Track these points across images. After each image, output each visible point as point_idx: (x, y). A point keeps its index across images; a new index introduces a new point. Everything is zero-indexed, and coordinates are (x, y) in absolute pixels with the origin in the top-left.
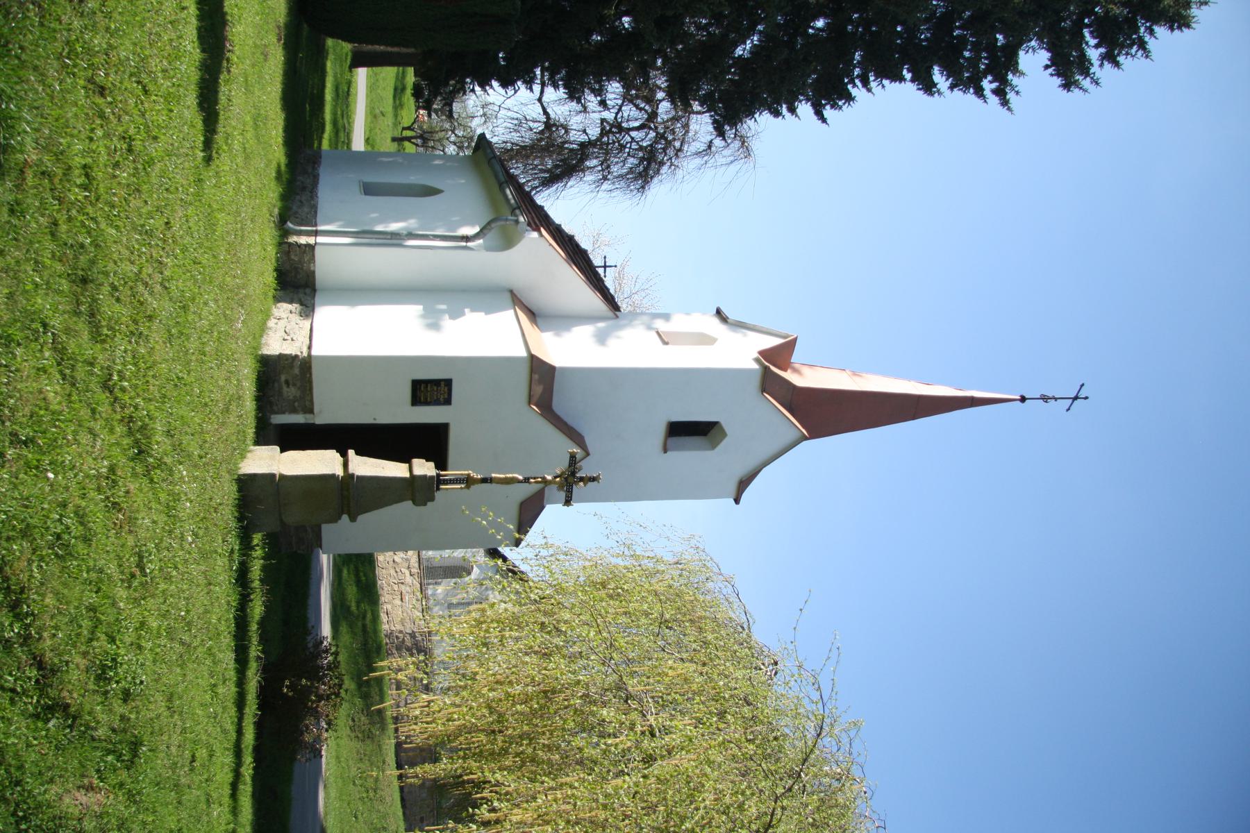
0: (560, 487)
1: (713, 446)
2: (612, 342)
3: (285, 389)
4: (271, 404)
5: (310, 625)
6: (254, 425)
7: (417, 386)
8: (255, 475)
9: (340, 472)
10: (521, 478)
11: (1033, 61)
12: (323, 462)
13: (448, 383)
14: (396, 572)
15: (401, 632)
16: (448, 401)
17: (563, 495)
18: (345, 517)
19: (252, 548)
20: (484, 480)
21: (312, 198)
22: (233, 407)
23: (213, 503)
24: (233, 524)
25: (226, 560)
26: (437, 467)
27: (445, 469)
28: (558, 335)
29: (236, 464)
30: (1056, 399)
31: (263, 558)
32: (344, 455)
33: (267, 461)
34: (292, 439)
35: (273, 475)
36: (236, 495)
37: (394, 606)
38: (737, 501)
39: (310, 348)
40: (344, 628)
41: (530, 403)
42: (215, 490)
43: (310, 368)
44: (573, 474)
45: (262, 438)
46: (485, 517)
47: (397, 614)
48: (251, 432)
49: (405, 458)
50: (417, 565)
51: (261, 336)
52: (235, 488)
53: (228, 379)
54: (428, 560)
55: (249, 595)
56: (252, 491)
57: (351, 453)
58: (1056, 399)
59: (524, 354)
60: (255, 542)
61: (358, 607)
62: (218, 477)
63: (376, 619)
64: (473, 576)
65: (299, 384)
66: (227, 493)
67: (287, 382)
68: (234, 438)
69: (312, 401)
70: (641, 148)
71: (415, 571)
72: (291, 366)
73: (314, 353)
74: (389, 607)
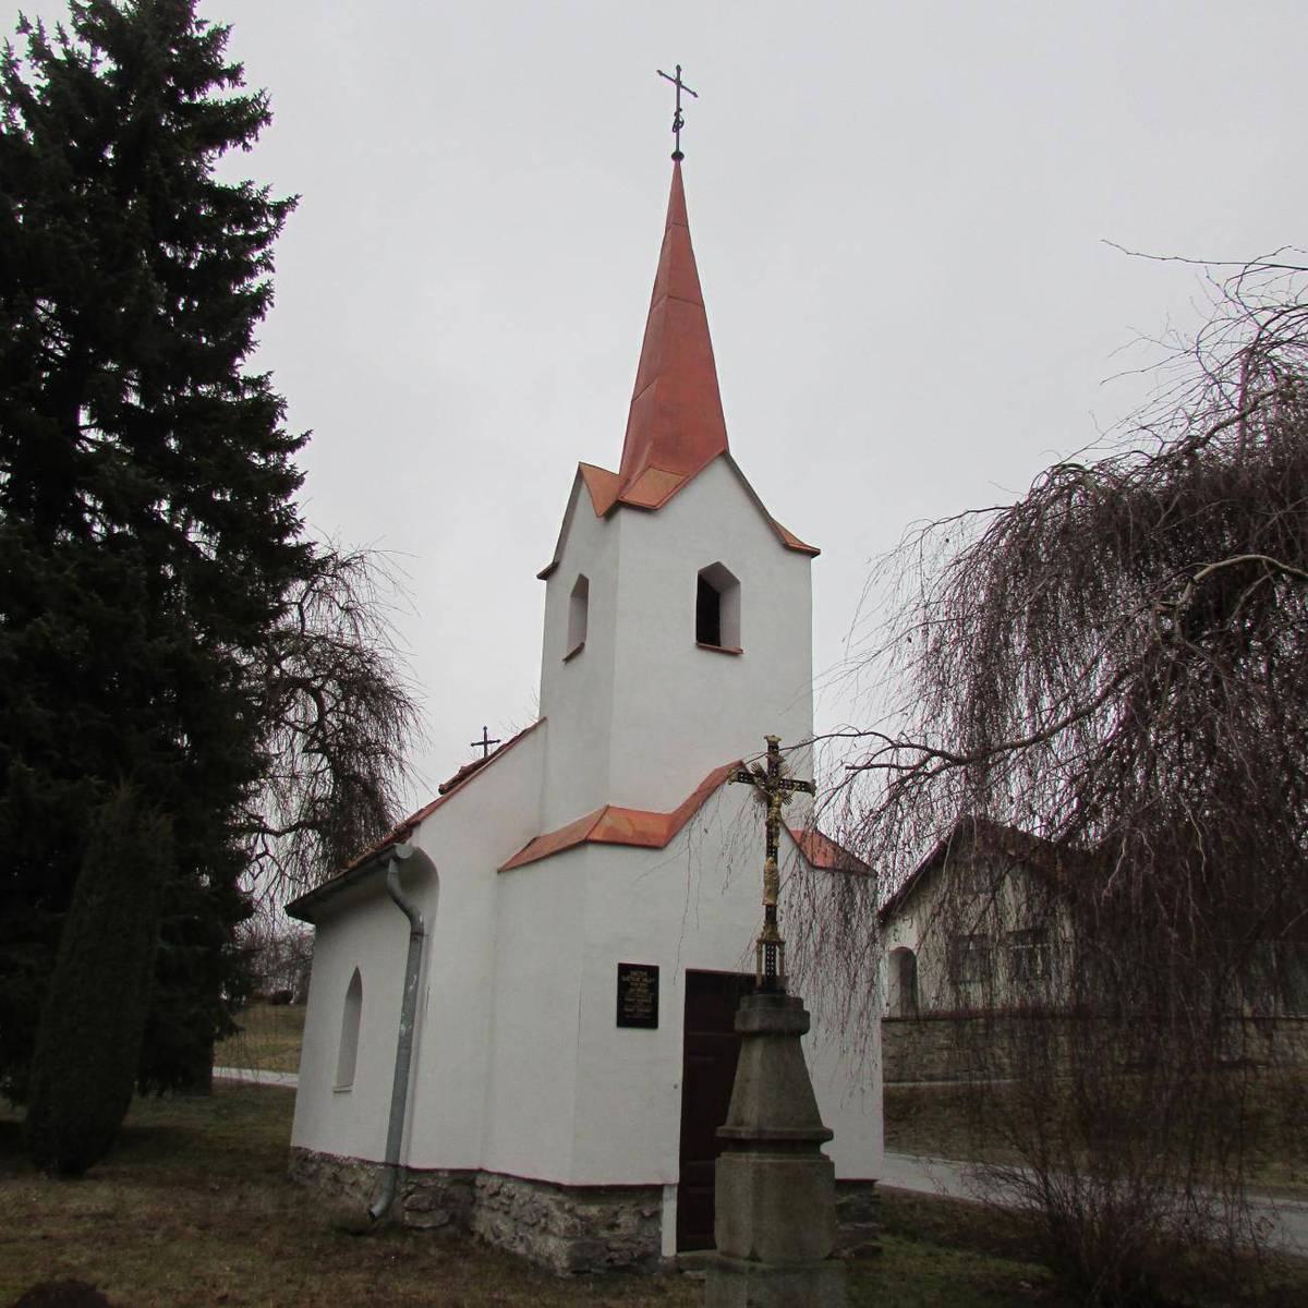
1: (732, 582)
11: (226, 168)
13: (624, 969)
16: (653, 972)
18: (825, 1148)
21: (350, 1167)
30: (679, 110)
38: (814, 553)
58: (679, 110)
70: (345, 698)
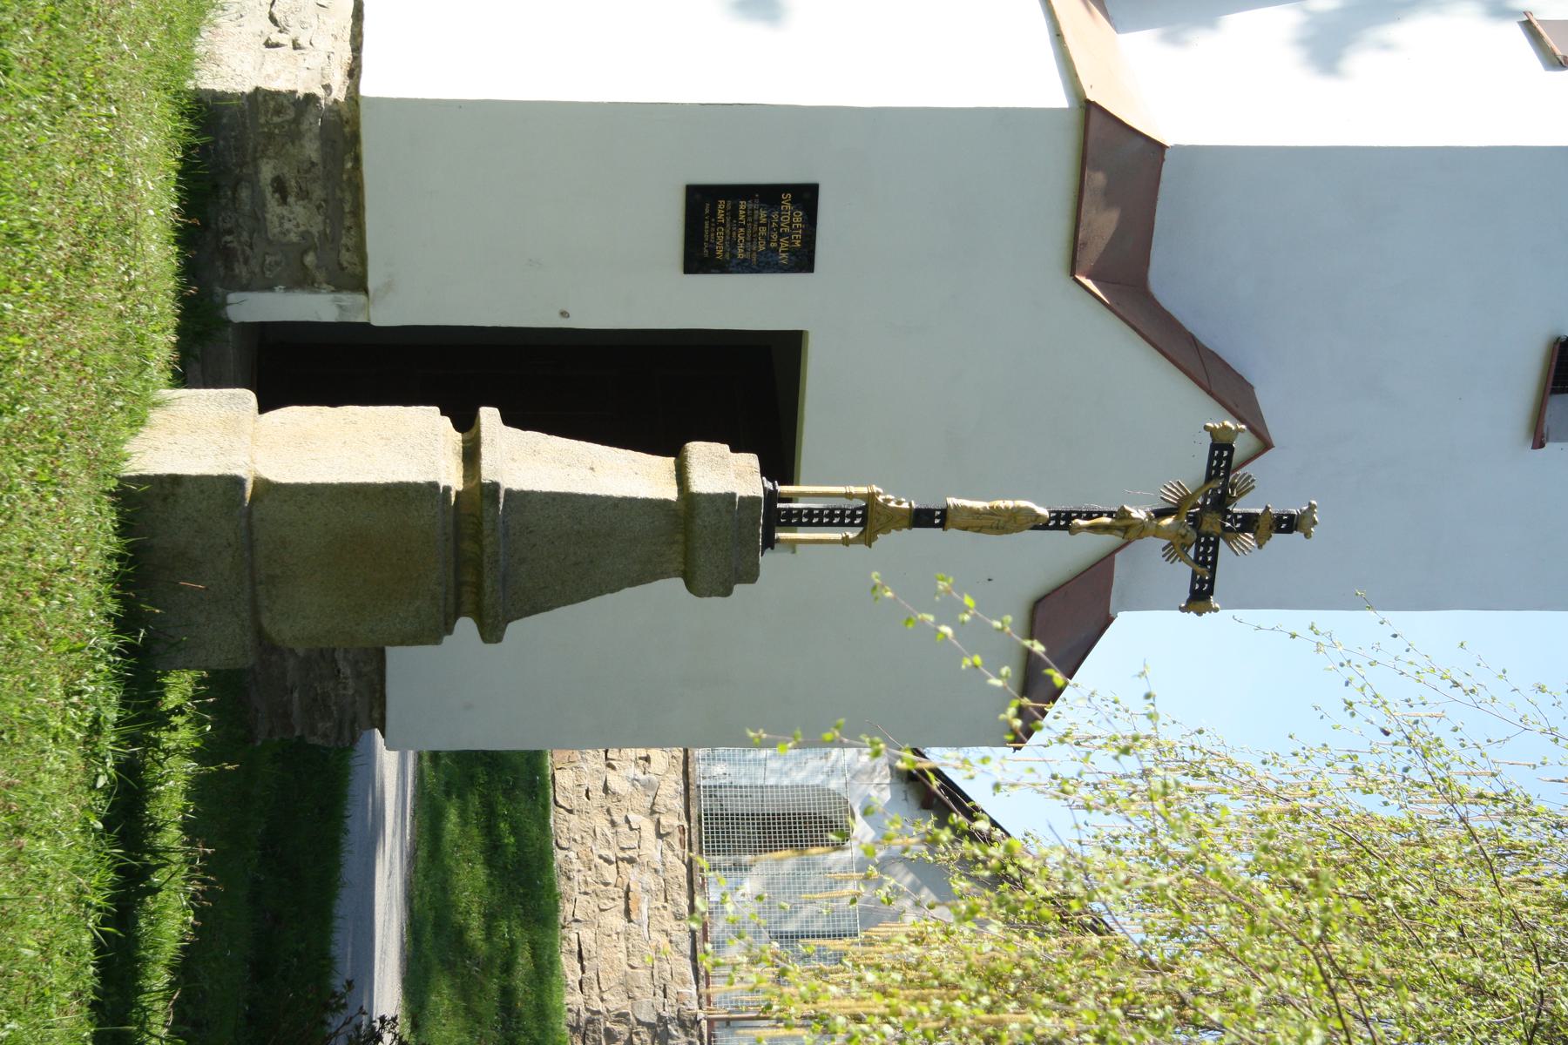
0: (1175, 549)
2: (1362, 62)
3: (273, 207)
4: (228, 255)
5: (338, 984)
6: (172, 321)
7: (704, 204)
8: (176, 480)
9: (452, 477)
10: (1043, 511)
12: (393, 445)
13: (806, 197)
14: (611, 811)
15: (622, 1017)
16: (803, 261)
17: (1181, 575)
18: (466, 627)
19: (162, 720)
20: (922, 518)
22: (104, 257)
23: (36, 565)
24: (101, 638)
25: (74, 755)
26: (767, 471)
27: (789, 480)
28: (1172, 39)
29: (112, 443)
31: (196, 755)
32: (465, 422)
33: (213, 435)
34: (297, 369)
35: (237, 482)
36: (114, 544)
37: (603, 934)
39: (354, 72)
40: (442, 998)
41: (1073, 273)
42: (43, 521)
43: (355, 139)
44: (1221, 503)
45: (207, 352)
46: (949, 611)
47: (610, 959)
48: (162, 345)
49: (664, 439)
50: (678, 804)
51: (195, 31)
52: (110, 520)
53: (86, 159)
54: (712, 791)
55: (149, 870)
56: (168, 541)
57: (489, 416)
59: (1056, 98)
60: (172, 699)
61: (489, 931)
62: (50, 481)
63: (544, 970)
64: (853, 852)
65: (318, 193)
66: (84, 540)
67: (280, 186)
68: (106, 357)
69: (360, 250)
71: (672, 821)
72: (294, 134)
73: (367, 89)
74: (587, 935)
